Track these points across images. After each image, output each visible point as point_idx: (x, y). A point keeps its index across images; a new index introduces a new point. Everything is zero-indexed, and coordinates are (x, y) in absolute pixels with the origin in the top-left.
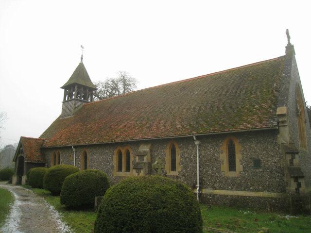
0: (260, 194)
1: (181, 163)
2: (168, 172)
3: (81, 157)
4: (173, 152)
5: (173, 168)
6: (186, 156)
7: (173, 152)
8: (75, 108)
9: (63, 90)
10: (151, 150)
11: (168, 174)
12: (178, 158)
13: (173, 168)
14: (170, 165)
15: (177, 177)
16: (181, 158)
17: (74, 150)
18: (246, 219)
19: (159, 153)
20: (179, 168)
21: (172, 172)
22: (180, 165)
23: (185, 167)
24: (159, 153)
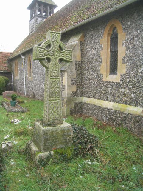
0: (119, 106)
1: (127, 58)
2: (104, 76)
3: (27, 61)
4: (114, 41)
5: (114, 69)
6: (136, 43)
7: (114, 41)
8: (37, 23)
9: (29, 11)
10: (82, 44)
11: (104, 80)
12: (122, 51)
13: (114, 69)
14: (109, 64)
15: (118, 85)
16: (127, 48)
17: (23, 57)
18: (42, 155)
19: (92, 47)
20: (122, 69)
21: (112, 75)
22: (124, 62)
23: (134, 67)
24: (92, 47)
